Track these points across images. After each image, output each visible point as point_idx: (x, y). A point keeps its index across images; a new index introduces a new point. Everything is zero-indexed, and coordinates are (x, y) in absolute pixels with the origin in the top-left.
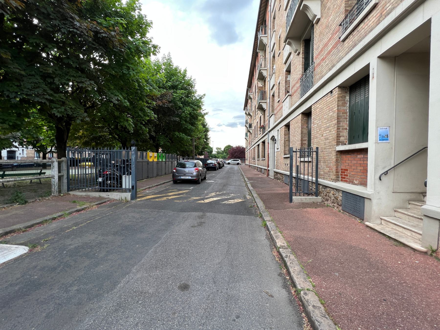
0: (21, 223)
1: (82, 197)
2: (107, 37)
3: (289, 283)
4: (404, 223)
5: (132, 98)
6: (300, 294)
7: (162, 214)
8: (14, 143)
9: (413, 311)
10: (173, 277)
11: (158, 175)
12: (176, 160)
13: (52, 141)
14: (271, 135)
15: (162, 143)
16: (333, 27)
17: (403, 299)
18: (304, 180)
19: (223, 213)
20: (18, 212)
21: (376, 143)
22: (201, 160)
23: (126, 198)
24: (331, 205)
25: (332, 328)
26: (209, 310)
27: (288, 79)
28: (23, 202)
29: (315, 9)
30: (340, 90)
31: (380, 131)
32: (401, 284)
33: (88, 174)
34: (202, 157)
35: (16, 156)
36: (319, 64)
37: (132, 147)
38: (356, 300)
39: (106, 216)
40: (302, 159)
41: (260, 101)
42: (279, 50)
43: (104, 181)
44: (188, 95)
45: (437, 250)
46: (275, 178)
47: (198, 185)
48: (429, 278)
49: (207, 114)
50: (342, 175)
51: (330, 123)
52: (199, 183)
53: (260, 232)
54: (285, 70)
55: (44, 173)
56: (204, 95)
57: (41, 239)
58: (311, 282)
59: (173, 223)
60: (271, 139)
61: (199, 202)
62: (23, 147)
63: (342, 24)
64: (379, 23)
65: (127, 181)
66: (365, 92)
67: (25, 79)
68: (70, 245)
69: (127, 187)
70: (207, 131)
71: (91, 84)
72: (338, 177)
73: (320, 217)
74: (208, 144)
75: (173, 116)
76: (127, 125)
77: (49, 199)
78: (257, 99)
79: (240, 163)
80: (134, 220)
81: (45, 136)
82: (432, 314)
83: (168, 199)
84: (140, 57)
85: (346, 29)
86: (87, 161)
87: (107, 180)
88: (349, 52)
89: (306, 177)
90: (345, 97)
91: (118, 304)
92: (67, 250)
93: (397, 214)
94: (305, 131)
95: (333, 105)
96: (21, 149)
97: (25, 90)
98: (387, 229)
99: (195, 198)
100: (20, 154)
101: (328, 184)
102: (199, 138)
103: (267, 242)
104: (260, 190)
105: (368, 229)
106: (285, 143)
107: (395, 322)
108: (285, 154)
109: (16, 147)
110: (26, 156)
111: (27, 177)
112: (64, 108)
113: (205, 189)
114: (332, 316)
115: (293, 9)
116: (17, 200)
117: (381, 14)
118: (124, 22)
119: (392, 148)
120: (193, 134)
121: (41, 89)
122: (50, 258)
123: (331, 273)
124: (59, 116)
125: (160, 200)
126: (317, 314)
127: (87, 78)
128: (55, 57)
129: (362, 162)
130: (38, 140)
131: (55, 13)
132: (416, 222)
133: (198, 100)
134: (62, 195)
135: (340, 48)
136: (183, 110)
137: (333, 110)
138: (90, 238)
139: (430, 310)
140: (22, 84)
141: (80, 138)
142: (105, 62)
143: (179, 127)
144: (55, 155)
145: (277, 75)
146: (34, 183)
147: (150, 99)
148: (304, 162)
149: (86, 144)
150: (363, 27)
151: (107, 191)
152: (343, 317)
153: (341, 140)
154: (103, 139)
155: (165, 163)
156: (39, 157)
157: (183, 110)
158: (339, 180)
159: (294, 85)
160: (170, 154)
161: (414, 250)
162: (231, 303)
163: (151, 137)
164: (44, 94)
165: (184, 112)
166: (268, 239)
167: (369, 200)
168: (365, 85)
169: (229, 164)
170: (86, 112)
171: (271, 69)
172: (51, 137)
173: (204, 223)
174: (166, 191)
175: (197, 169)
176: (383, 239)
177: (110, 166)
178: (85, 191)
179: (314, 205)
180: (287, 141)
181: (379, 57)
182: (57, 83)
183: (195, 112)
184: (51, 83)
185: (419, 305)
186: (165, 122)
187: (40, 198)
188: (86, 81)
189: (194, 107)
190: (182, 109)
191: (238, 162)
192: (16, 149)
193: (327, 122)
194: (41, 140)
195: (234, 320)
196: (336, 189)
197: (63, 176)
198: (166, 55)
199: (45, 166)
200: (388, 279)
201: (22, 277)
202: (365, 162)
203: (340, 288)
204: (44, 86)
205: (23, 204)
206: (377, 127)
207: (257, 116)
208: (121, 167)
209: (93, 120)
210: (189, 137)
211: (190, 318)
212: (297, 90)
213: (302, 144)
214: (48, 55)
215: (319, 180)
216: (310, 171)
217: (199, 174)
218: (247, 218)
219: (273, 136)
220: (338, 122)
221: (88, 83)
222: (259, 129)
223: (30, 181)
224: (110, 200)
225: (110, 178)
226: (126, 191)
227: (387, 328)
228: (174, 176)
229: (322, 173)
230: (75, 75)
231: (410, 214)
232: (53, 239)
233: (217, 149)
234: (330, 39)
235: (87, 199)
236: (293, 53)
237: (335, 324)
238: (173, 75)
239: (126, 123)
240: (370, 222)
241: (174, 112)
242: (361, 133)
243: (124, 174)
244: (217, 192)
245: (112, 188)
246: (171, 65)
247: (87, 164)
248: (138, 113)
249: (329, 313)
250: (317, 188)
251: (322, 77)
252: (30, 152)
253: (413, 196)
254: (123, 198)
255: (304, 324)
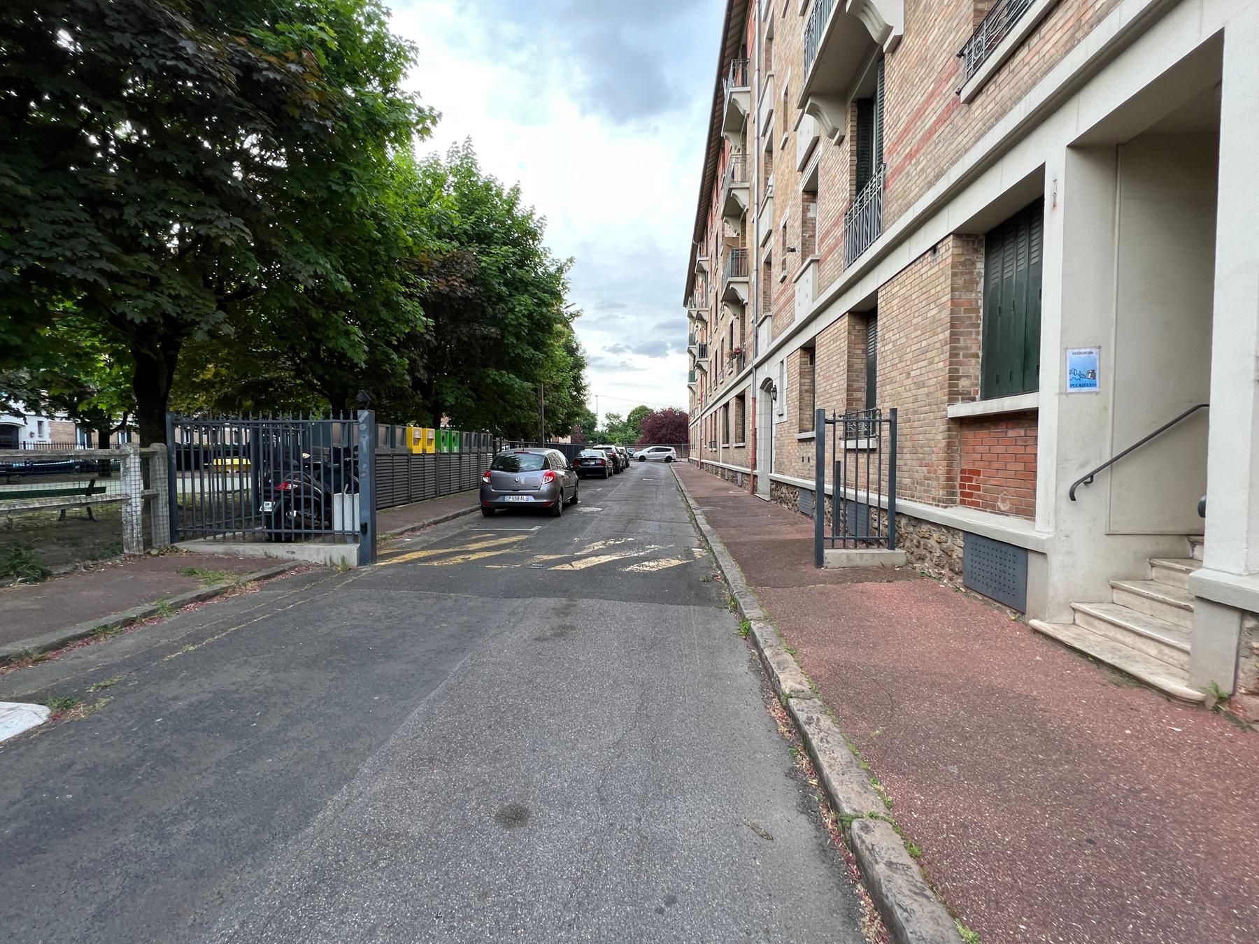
0: (28, 636)
1: (213, 559)
2: (281, 84)
3: (819, 799)
4: (1136, 620)
5: (358, 271)
6: (850, 828)
7: (449, 603)
8: (11, 403)
9: (1170, 870)
10: (481, 789)
11: (437, 494)
12: (491, 449)
13: (123, 397)
14: (761, 375)
15: (451, 400)
16: (940, 61)
17: (1141, 836)
18: (856, 502)
19: (627, 599)
20: (20, 604)
21: (1060, 394)
22: (562, 448)
23: (343, 559)
24: (933, 572)
25: (944, 926)
26: (585, 881)
27: (810, 215)
28: (38, 573)
29: (887, 5)
30: (959, 243)
31: (1072, 359)
32: (1133, 792)
33: (233, 492)
34: (567, 440)
35: (21, 440)
36: (899, 170)
37: (359, 412)
38: (1009, 842)
39: (285, 613)
40: (851, 444)
41: (730, 279)
42: (785, 129)
43: (278, 513)
44: (522, 261)
45: (1233, 694)
46: (773, 498)
47: (554, 521)
48: (1213, 774)
49: (578, 314)
50: (963, 488)
51: (931, 341)
52: (558, 515)
53: (731, 651)
54: (801, 189)
55: (103, 490)
56: (571, 260)
57: (87, 682)
58: (880, 793)
59: (483, 630)
60: (762, 388)
61: (558, 568)
62: (38, 414)
63: (966, 52)
64: (1073, 47)
65: (347, 511)
66: (1030, 247)
67: (32, 209)
68: (175, 698)
69: (348, 528)
70: (579, 365)
71: (233, 228)
72: (953, 494)
73: (901, 605)
74: (582, 402)
75: (480, 324)
76: (345, 346)
77: (115, 566)
78: (720, 272)
79: (674, 456)
80: (369, 623)
81: (102, 380)
82: (1226, 879)
83: (467, 561)
84: (381, 146)
85: (977, 66)
86: (228, 454)
87: (287, 508)
88: (984, 133)
89: (862, 494)
90: (973, 263)
91: (316, 870)
92: (165, 713)
93: (1117, 596)
94: (860, 364)
95: (939, 288)
96: (32, 421)
97: (35, 243)
98: (1092, 637)
99: (545, 557)
100: (32, 434)
101: (925, 513)
102: (557, 388)
103: (751, 681)
104: (732, 531)
105: (1037, 639)
106: (801, 399)
107: (1123, 905)
108: (801, 431)
109: (17, 414)
110: (49, 441)
111: (47, 502)
112: (152, 297)
113: (575, 532)
114: (942, 893)
115: (825, 8)
116: (18, 569)
117: (1079, 20)
118: (330, 37)
119: (1105, 409)
120: (539, 372)
121: (82, 239)
122: (115, 739)
123: (936, 767)
124: (137, 321)
125: (444, 563)
126: (901, 888)
127: (224, 207)
128: (124, 145)
129: (1021, 450)
130: (83, 394)
131: (118, 12)
132: (1171, 617)
133: (550, 276)
134: (154, 552)
135: (959, 121)
136: (510, 305)
137: (938, 302)
138: (234, 676)
139: (1217, 867)
140: (23, 223)
141: (206, 386)
142: (277, 164)
143: (497, 353)
144: (136, 438)
145: (777, 202)
146: (72, 518)
147: (413, 271)
148: (857, 451)
149: (227, 405)
150: (1042, 42)
151: (288, 540)
152: (975, 895)
153: (960, 388)
154: (276, 390)
155: (460, 458)
156: (90, 445)
157: (510, 305)
158: (954, 502)
159: (828, 232)
160: (473, 434)
161: (1169, 696)
162: (650, 859)
163: (417, 384)
164: (91, 257)
165: (512, 310)
166: (757, 672)
167: (1040, 557)
168: (1030, 229)
169: (642, 459)
170: (221, 306)
171: (762, 185)
172: (120, 384)
173: (572, 628)
174: (464, 538)
175: (550, 475)
176: (1082, 667)
177: (297, 468)
178: (224, 540)
179: (885, 573)
180: (808, 391)
181: (1071, 146)
182: (133, 221)
183: (544, 310)
184: (113, 223)
185: (1187, 854)
186: (458, 339)
187: (90, 562)
188: (219, 217)
189: (540, 294)
190: (506, 304)
191: (668, 454)
192: (20, 421)
193: (922, 337)
194: (91, 394)
195: (661, 911)
196: (946, 527)
197: (156, 496)
198: (460, 144)
199: (107, 469)
200: (1098, 780)
201: (25, 797)
202: (1029, 450)
203: (964, 809)
204: (93, 231)
205: (36, 580)
206: (1065, 349)
207: (721, 324)
208: (327, 470)
209: (245, 335)
210: (528, 385)
211: (530, 906)
212: (836, 245)
213: (850, 401)
214: (105, 139)
215: (898, 501)
216: (874, 477)
217: (557, 489)
218: (695, 613)
219: (769, 379)
220: (954, 337)
221: (226, 223)
222: (726, 359)
223: (57, 512)
224: (296, 566)
225: (297, 501)
226: (343, 538)
227: (1099, 922)
228: (484, 494)
229: (907, 481)
230: (185, 200)
231: (1155, 595)
232: (125, 683)
233: (607, 417)
234: (932, 95)
235: (232, 563)
236: (824, 138)
237: (954, 916)
238: (479, 202)
239: (343, 343)
240: (1042, 620)
241: (484, 313)
242: (1018, 364)
243: (338, 490)
244: (609, 538)
245: (303, 531)
246: (474, 175)
247: (228, 461)
248: (378, 313)
249: (933, 881)
250: (893, 526)
251: (908, 206)
252: (60, 428)
253: (1165, 545)
254: (337, 560)
255: (863, 915)
